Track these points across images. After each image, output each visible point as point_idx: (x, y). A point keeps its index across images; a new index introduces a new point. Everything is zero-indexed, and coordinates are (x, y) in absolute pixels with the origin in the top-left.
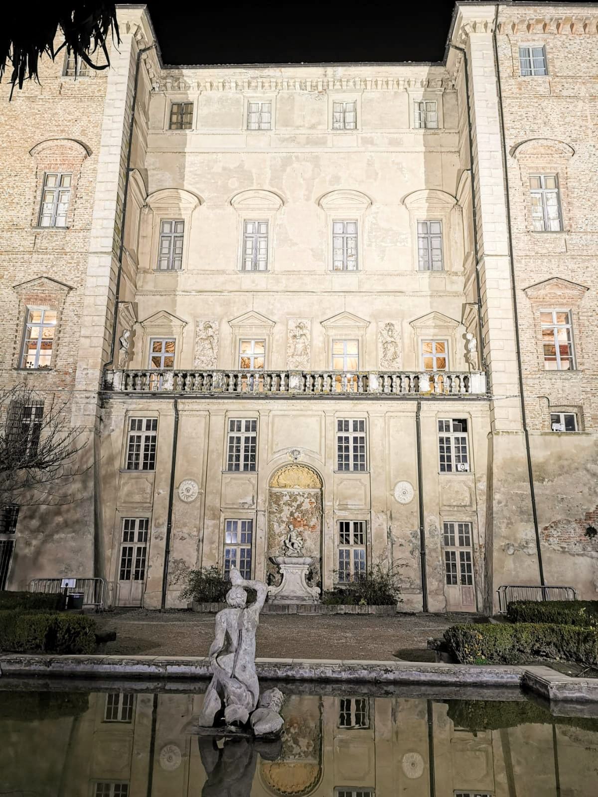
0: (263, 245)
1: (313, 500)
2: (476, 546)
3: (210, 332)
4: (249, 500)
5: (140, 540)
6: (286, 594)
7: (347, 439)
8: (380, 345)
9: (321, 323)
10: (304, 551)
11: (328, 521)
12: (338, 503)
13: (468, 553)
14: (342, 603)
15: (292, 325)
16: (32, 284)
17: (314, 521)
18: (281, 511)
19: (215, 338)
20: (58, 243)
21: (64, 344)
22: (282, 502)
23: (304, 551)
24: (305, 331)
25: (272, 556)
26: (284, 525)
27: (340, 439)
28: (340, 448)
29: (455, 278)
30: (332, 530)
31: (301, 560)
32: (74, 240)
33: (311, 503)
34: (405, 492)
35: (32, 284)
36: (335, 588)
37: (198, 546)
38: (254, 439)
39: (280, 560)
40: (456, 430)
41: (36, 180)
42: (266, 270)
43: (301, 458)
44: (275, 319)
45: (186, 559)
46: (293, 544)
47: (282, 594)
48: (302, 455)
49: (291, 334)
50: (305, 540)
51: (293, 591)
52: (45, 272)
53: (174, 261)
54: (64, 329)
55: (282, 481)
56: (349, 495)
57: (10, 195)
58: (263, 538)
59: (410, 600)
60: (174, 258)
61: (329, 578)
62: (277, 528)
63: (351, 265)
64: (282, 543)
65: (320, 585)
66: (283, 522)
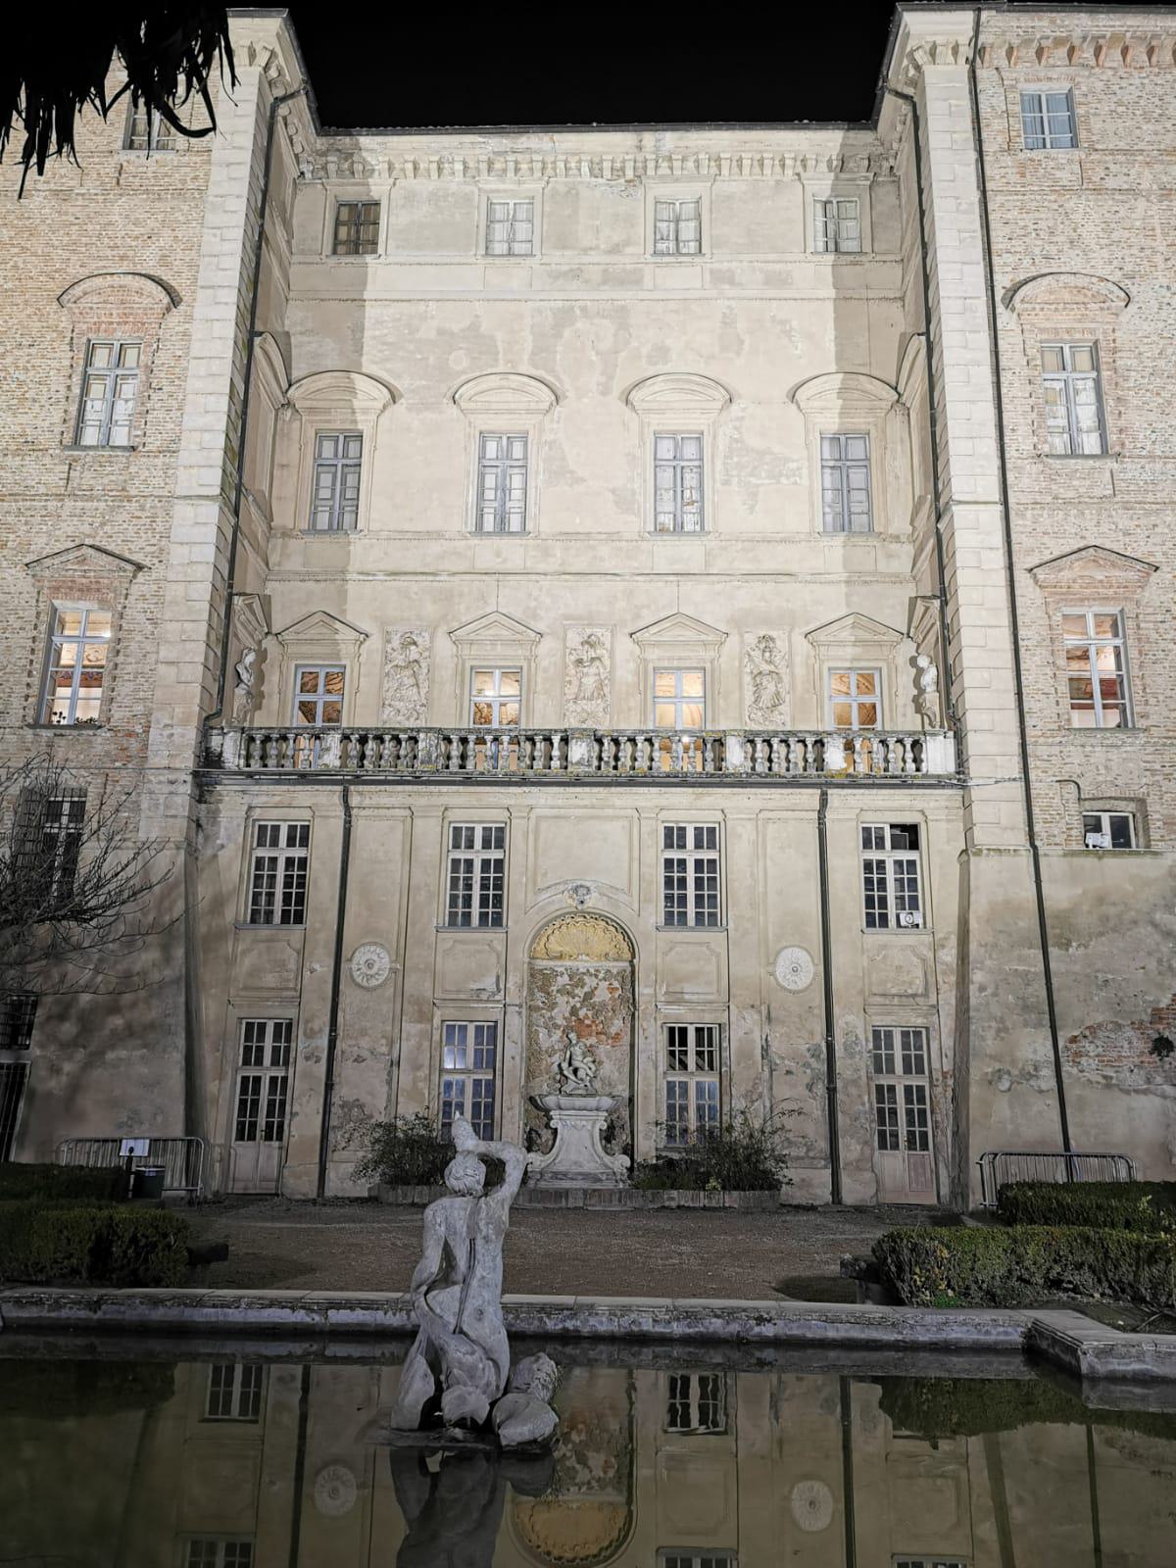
0: (517, 481)
1: (616, 984)
4: (489, 983)
5: (275, 1062)
6: (562, 1169)
7: (682, 863)
8: (748, 679)
10: (597, 1084)
11: (645, 1025)
12: (664, 990)
13: (920, 1089)
14: (673, 1187)
15: (574, 639)
16: (63, 559)
17: (617, 1025)
18: (552, 1006)
20: (113, 478)
21: (126, 677)
22: (555, 988)
23: (597, 1084)
25: (535, 1093)
26: (559, 1033)
27: (669, 863)
28: (669, 882)
30: (653, 1044)
31: (592, 1102)
32: (145, 473)
33: (612, 990)
34: (797, 968)
35: (63, 559)
36: (658, 1158)
37: (390, 1074)
38: (499, 863)
39: (550, 1101)
40: (896, 845)
41: (71, 354)
42: (524, 532)
43: (593, 902)
44: (541, 627)
45: (365, 1099)
46: (575, 1071)
47: (555, 1169)
48: (594, 895)
50: (601, 1063)
51: (576, 1163)
52: (89, 536)
53: (342, 514)
54: (126, 647)
55: (555, 947)
56: (686, 973)
57: (21, 383)
58: (518, 1058)
61: (647, 1137)
62: (547, 1040)
63: (690, 522)
64: (555, 1068)
65: (629, 1150)
66: (556, 1026)
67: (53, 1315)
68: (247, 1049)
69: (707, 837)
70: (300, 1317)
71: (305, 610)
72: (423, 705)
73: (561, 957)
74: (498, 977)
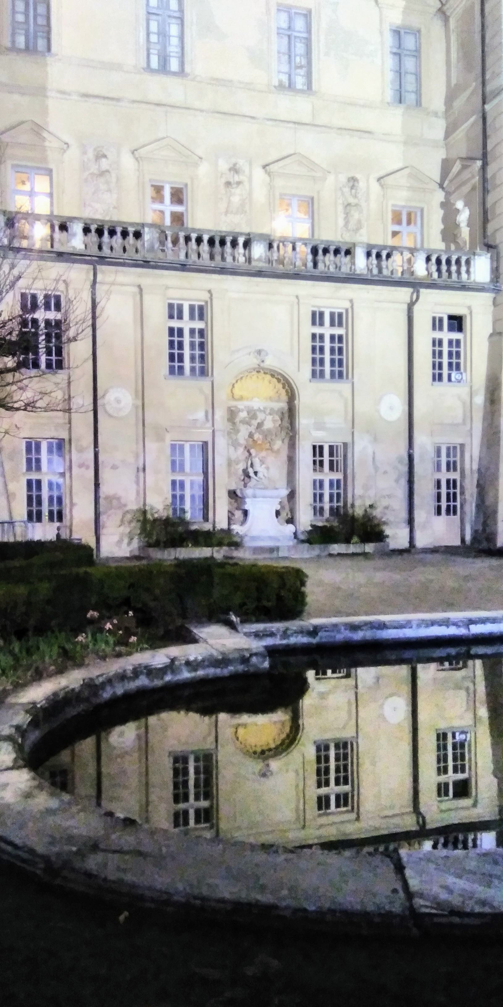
0: (174, 30)
2: (467, 472)
3: (104, 164)
8: (340, 208)
9: (264, 167)
13: (455, 481)
15: (223, 166)
18: (238, 431)
19: (114, 175)
24: (242, 178)
27: (171, 331)
29: (434, 119)
30: (305, 456)
33: (274, 421)
34: (393, 408)
37: (137, 477)
38: (202, 333)
40: (451, 329)
42: (182, 73)
43: (270, 362)
44: (200, 152)
45: (121, 493)
46: (256, 473)
49: (223, 180)
53: (36, 37)
56: (323, 411)
59: (397, 537)
60: (35, 32)
63: (300, 82)
66: (240, 445)
67: (284, 642)
68: (29, 461)
69: (338, 319)
70: (452, 631)
71: (14, 119)
72: (115, 208)
73: (241, 398)
74: (207, 412)
